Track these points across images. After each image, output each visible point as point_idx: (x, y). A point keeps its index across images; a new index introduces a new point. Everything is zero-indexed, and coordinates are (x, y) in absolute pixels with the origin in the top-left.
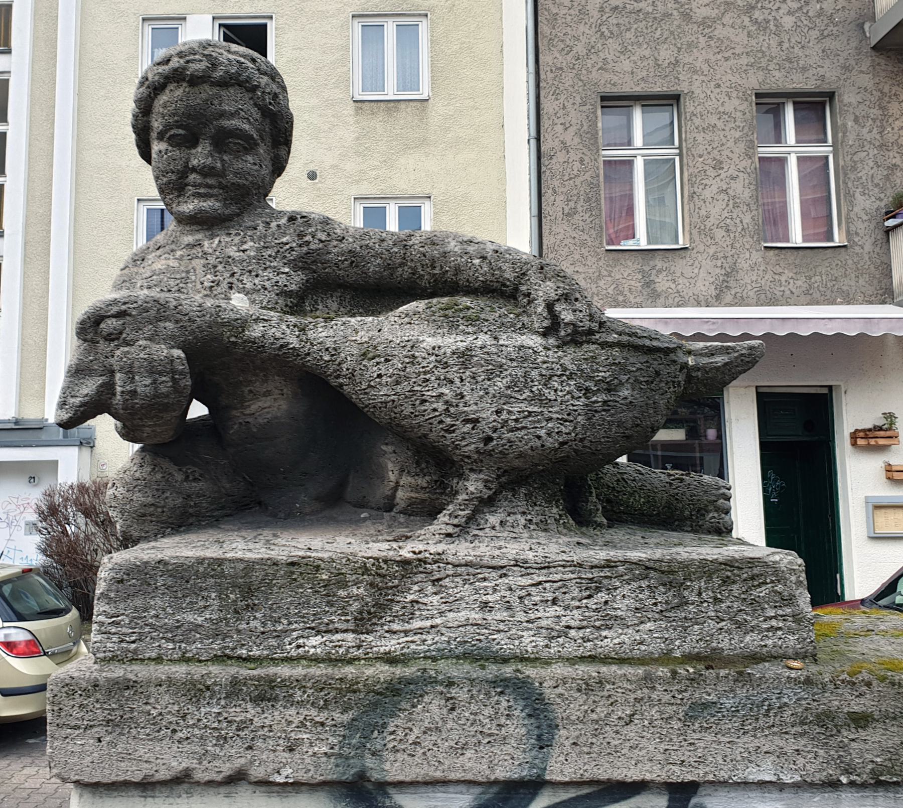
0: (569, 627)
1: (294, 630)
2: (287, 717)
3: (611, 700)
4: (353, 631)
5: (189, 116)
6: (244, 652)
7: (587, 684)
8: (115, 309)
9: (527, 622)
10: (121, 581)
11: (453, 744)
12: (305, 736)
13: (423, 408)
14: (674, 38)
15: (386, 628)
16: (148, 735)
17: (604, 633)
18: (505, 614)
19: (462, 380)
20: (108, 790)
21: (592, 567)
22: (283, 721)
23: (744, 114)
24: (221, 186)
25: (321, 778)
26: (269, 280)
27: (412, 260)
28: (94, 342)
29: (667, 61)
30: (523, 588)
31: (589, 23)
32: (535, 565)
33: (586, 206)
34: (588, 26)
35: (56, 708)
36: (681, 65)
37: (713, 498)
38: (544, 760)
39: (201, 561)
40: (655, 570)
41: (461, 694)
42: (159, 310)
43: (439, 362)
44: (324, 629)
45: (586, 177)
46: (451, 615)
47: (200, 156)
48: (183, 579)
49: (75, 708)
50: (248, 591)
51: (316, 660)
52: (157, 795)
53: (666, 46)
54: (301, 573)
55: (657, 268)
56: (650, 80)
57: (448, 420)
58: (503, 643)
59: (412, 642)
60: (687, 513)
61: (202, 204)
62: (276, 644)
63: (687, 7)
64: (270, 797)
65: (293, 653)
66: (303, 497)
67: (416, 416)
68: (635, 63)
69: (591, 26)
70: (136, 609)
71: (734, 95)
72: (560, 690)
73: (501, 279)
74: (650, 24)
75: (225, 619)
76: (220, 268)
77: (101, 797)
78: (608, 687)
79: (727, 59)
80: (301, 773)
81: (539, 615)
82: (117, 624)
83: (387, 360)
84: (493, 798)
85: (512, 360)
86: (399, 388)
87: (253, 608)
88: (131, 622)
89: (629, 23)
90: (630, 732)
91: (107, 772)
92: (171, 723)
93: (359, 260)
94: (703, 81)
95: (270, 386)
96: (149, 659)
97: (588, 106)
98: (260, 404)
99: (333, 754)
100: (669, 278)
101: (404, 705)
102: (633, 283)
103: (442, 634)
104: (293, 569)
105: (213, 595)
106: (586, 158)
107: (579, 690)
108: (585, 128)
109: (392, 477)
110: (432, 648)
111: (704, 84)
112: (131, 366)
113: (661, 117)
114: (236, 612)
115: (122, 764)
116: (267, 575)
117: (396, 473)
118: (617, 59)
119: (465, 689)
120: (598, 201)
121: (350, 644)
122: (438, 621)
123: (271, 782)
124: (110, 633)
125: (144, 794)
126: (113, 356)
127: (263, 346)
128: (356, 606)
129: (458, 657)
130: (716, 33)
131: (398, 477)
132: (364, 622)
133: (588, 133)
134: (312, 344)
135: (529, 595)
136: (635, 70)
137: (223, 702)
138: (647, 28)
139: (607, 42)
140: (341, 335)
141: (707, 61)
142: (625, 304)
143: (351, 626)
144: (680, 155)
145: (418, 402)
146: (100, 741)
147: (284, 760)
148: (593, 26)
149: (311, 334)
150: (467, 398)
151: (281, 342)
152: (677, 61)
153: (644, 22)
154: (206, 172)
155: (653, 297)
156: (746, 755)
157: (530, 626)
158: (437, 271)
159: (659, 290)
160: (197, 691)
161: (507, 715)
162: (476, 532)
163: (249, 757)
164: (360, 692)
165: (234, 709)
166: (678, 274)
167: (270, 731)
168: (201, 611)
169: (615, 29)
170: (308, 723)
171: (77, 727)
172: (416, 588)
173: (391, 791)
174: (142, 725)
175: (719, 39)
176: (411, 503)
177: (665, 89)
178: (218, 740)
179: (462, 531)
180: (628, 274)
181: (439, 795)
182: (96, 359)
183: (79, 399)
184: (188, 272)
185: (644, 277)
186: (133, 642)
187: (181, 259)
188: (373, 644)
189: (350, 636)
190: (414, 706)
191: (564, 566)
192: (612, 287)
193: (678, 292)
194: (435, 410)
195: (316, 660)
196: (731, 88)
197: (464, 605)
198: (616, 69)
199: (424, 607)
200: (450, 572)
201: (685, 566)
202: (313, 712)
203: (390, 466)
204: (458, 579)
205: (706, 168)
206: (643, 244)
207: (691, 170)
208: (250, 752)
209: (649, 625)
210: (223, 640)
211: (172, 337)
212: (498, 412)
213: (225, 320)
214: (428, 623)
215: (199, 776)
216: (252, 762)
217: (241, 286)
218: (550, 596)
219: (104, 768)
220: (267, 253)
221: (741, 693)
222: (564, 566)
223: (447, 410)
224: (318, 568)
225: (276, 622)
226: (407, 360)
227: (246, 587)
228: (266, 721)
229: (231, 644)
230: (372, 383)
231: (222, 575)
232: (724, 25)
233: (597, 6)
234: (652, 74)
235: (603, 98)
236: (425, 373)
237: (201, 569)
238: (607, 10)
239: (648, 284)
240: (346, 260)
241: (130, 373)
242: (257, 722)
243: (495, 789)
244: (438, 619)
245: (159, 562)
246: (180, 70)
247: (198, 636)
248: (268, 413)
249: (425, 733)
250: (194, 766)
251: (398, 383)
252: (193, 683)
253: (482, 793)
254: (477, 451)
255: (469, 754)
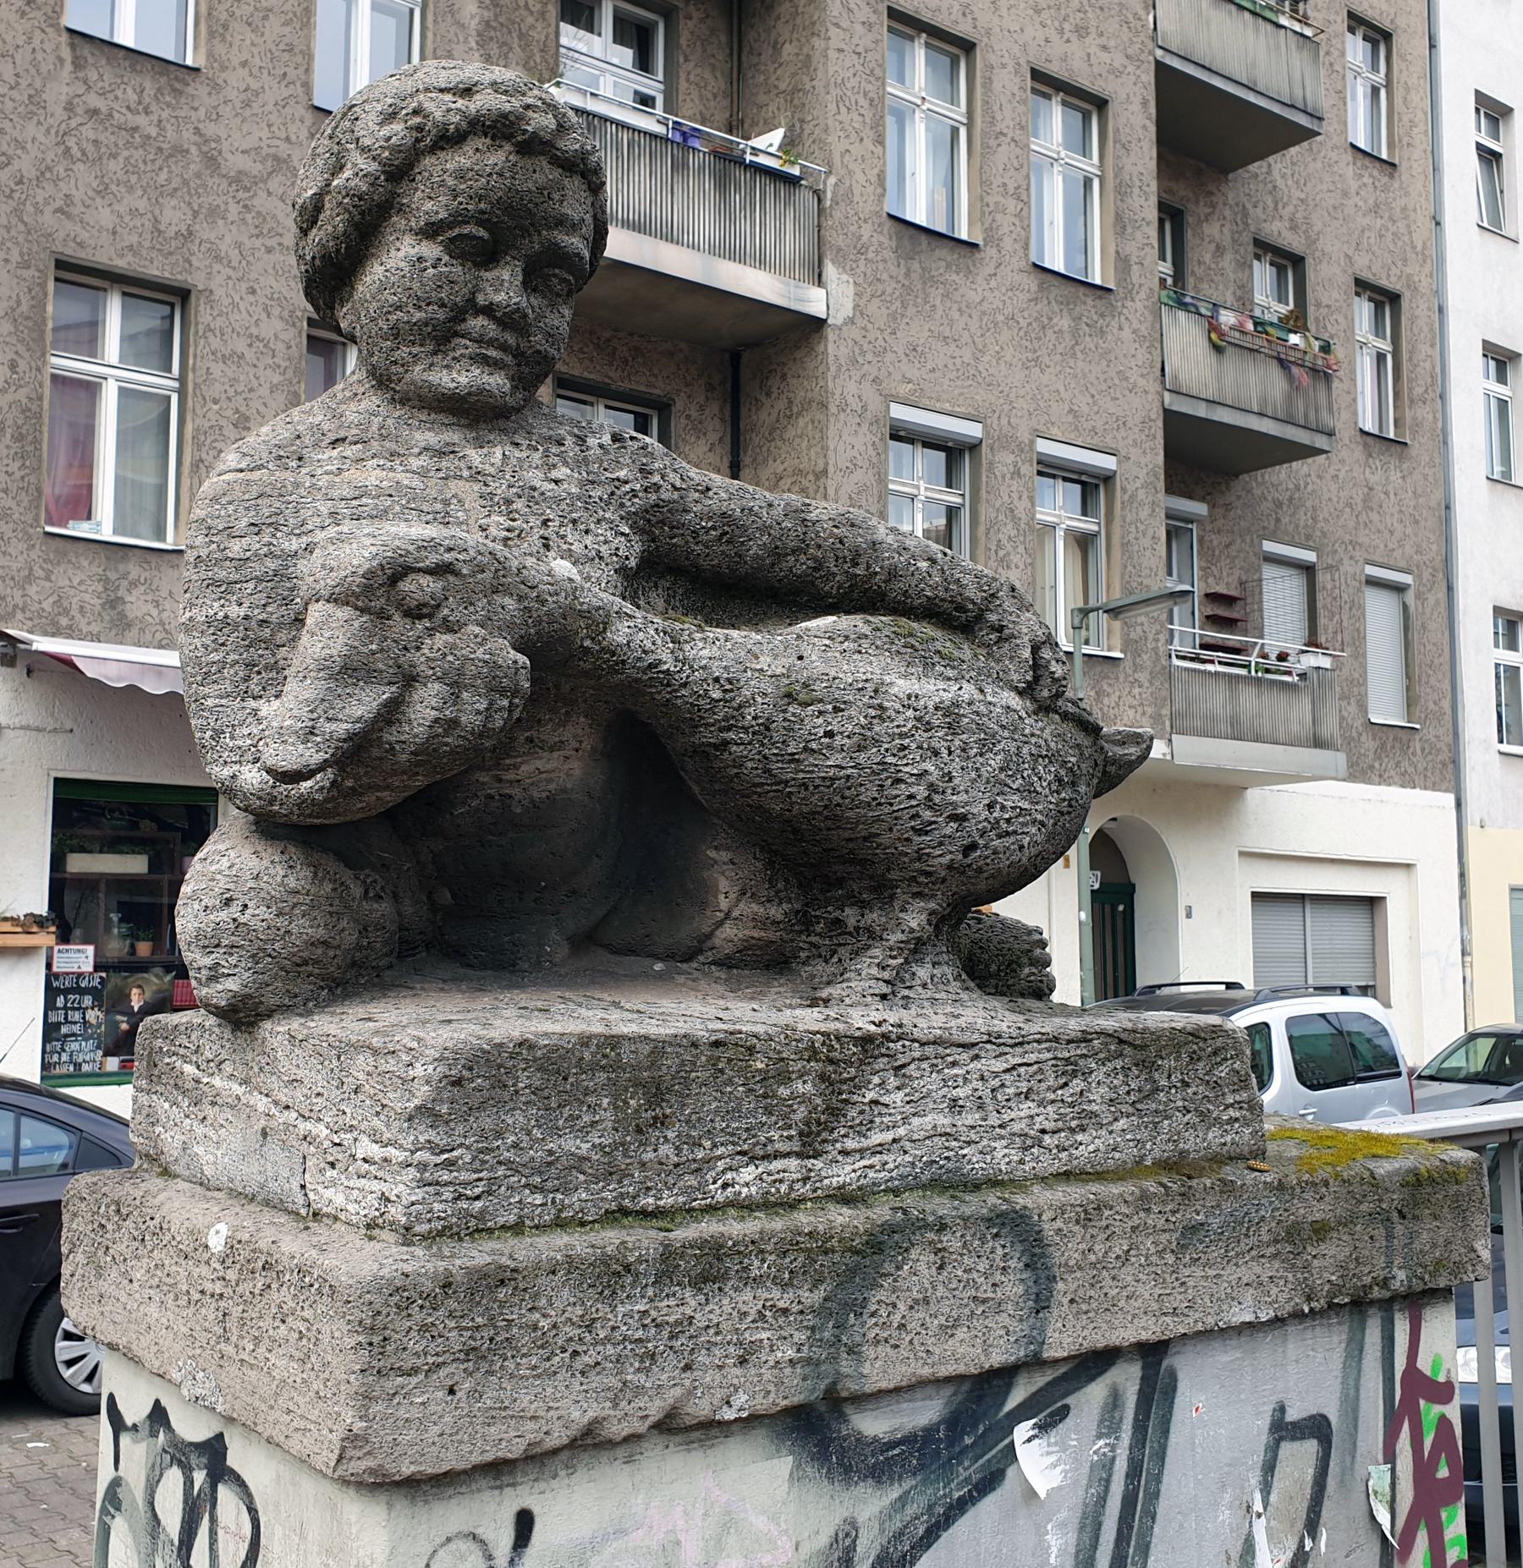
0: (1043, 1131)
1: (720, 1158)
2: (740, 1305)
3: (1108, 1232)
4: (799, 1155)
5: (508, 209)
6: (651, 1200)
7: (1086, 1211)
8: (432, 559)
9: (1000, 1126)
10: (458, 1082)
11: (942, 1320)
12: (764, 1335)
13: (895, 792)
14: (189, 193)
15: (838, 1146)
16: (535, 1368)
17: (1079, 1137)
18: (977, 1116)
19: (950, 753)
20: (439, 1487)
21: (1069, 1042)
22: (735, 1313)
23: (289, 347)
24: (518, 354)
25: (785, 1402)
26: (606, 542)
27: (819, 547)
28: (382, 615)
29: (174, 229)
30: (996, 1075)
31: (46, 126)
32: (1010, 1041)
33: (15, 447)
34: (43, 129)
35: (376, 1339)
36: (197, 242)
37: (1027, 947)
38: (1042, 1331)
39: (585, 1040)
40: (1130, 1044)
41: (951, 1241)
42: (497, 571)
43: (918, 719)
44: (761, 1153)
45: (18, 396)
46: (916, 1121)
47: (504, 286)
48: (558, 1072)
49: (413, 1334)
50: (656, 1093)
51: (746, 1207)
52: (519, 1480)
53: (173, 202)
54: (730, 1060)
55: (131, 577)
56: (144, 252)
57: (927, 815)
58: (975, 1162)
59: (871, 1167)
60: (994, 967)
61: (486, 378)
62: (695, 1183)
63: (213, 145)
64: (689, 1451)
65: (720, 1197)
66: (554, 935)
67: (880, 804)
68: (120, 216)
69: (48, 131)
70: (483, 1137)
71: (276, 311)
72: (1059, 1224)
73: (959, 599)
74: (152, 157)
75: (623, 1144)
76: (519, 505)
77: (426, 1502)
78: (1107, 1213)
79: (269, 251)
80: (759, 1399)
81: (1013, 1115)
82: (450, 1164)
83: (836, 710)
84: (966, 1400)
85: (1003, 727)
86: (862, 758)
87: (661, 1122)
88: (474, 1159)
89: (116, 145)
90: (1127, 1275)
91: (466, 1448)
92: (571, 1339)
93: (737, 532)
94: (229, 278)
95: (567, 733)
96: (502, 1227)
97: (32, 272)
98: (539, 764)
99: (800, 1360)
100: (150, 598)
101: (888, 1267)
102: (87, 597)
103: (905, 1152)
104: (717, 1052)
105: (606, 1101)
106: (20, 361)
107: (1077, 1222)
108: (24, 308)
109: (724, 904)
110: (894, 1174)
111: (231, 283)
112: (460, 672)
113: (150, 318)
114: (639, 1130)
115: (492, 1429)
116: (683, 1063)
117: (732, 896)
118: (89, 202)
119: (958, 1234)
120: (37, 442)
121: (795, 1176)
122: (901, 1131)
123: (719, 1422)
124: (438, 1183)
125: (498, 1483)
126: (418, 648)
127: (623, 662)
128: (801, 1113)
129: (924, 1187)
130: (256, 202)
131: (734, 903)
132: (810, 1143)
133: (27, 318)
134: (691, 667)
135: (1003, 1085)
136: (119, 229)
137: (650, 1292)
138: (145, 162)
139: (75, 168)
140: (733, 658)
141: (239, 245)
142: (70, 633)
143: (796, 1146)
144: (182, 393)
145: (889, 782)
146: (452, 1392)
147: (735, 1381)
148: (53, 132)
149: (689, 651)
150: (956, 781)
151: (651, 659)
152: (191, 233)
153: (141, 152)
154: (511, 320)
155: (120, 627)
156: (1229, 1290)
157: (1003, 1132)
158: (860, 571)
159: (131, 615)
160: (611, 1276)
161: (1004, 1268)
162: (906, 992)
163: (687, 1383)
164: (833, 1252)
165: (665, 1303)
166: (164, 594)
167: (717, 1334)
168: (584, 1132)
169: (90, 148)
170: (768, 1313)
171: (414, 1371)
172: (876, 1080)
173: (849, 1409)
174: (524, 1351)
175: (259, 213)
176: (747, 946)
177: (167, 275)
178: (642, 1361)
179: (893, 990)
180: (80, 583)
181: (905, 1405)
182: (382, 650)
183: (345, 726)
184: (446, 503)
185: (106, 589)
186: (477, 1198)
187: (423, 473)
188: (823, 1174)
189: (793, 1163)
190: (899, 1268)
191: (1038, 1042)
192: (51, 600)
193: (162, 623)
194: (911, 797)
195: (746, 1207)
196: (272, 299)
197: (931, 1106)
198: (86, 218)
199: (885, 1110)
200: (917, 1054)
201: (1156, 1035)
202: (776, 1293)
203: (723, 885)
204: (925, 1065)
205: (223, 422)
206: (107, 534)
207: (198, 421)
208: (688, 1374)
209: (1122, 1123)
210: (620, 1182)
211: (510, 626)
212: (990, 806)
213: (585, 607)
214: (889, 1136)
215: (617, 1429)
216: (691, 1392)
217: (565, 547)
218: (1024, 1087)
219: (461, 1442)
220: (597, 493)
221: (1227, 1207)
222: (1038, 1042)
223: (929, 798)
224: (751, 1050)
225: (694, 1144)
226: (873, 712)
227: (652, 1085)
228: (711, 1316)
229: (631, 1189)
230: (814, 746)
231: (616, 1066)
232: (270, 194)
233: (63, 98)
234: (147, 244)
235: (60, 264)
236: (901, 736)
237: (587, 1056)
238: (80, 111)
239: (113, 603)
240: (714, 528)
241: (456, 684)
242: (700, 1321)
243: (966, 1387)
244: (907, 1124)
245: (520, 1045)
246: (512, 118)
247: (582, 1177)
248: (550, 781)
249: (911, 1308)
250: (607, 1412)
251: (860, 748)
252: (605, 1260)
253: (955, 1394)
254: (950, 867)
255: (961, 1333)
